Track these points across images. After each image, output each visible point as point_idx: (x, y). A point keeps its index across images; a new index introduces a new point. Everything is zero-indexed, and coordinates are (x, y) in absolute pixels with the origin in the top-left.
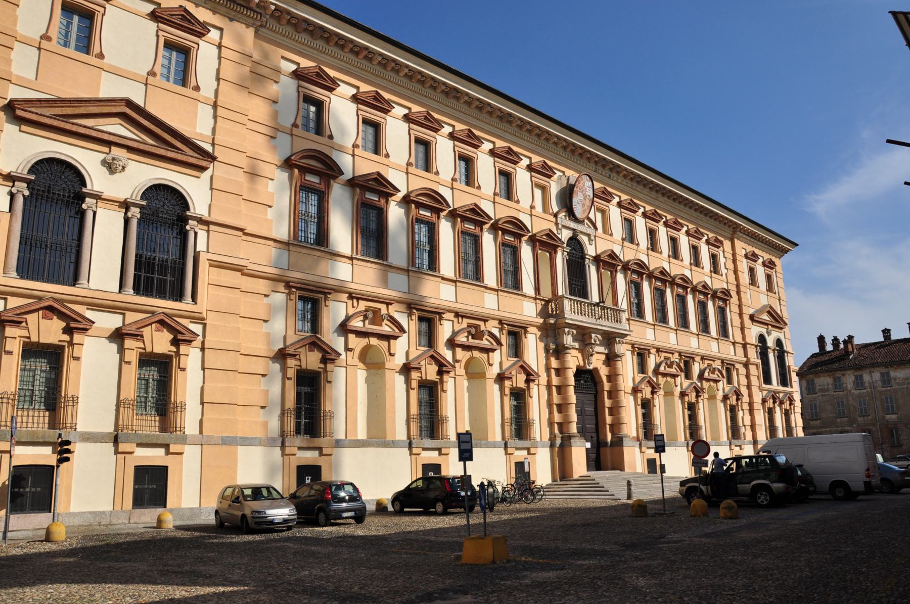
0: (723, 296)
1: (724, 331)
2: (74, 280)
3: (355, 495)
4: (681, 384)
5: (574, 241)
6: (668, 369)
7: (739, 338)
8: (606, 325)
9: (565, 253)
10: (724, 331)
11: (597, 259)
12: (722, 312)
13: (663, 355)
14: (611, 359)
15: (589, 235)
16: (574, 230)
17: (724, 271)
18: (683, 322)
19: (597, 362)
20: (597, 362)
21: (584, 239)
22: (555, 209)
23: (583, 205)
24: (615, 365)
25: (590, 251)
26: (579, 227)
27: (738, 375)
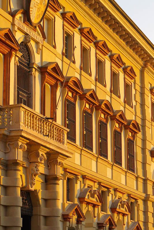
0: (134, 128)
1: (131, 167)
2: (92, 93)
3: (132, 139)
4: (98, 214)
5: (25, 47)
6: (91, 198)
7: (140, 173)
8: (53, 144)
9: (17, 58)
10: (131, 167)
11: (43, 70)
12: (130, 144)
13: (88, 183)
14: (49, 180)
15: (37, 43)
16: (26, 34)
17: (134, 103)
18: (102, 152)
19: (37, 185)
20: (37, 185)
21: (32, 44)
22: (13, 7)
23: (39, 9)
24: (54, 188)
25: (37, 60)
26: (33, 34)
27: (138, 210)
